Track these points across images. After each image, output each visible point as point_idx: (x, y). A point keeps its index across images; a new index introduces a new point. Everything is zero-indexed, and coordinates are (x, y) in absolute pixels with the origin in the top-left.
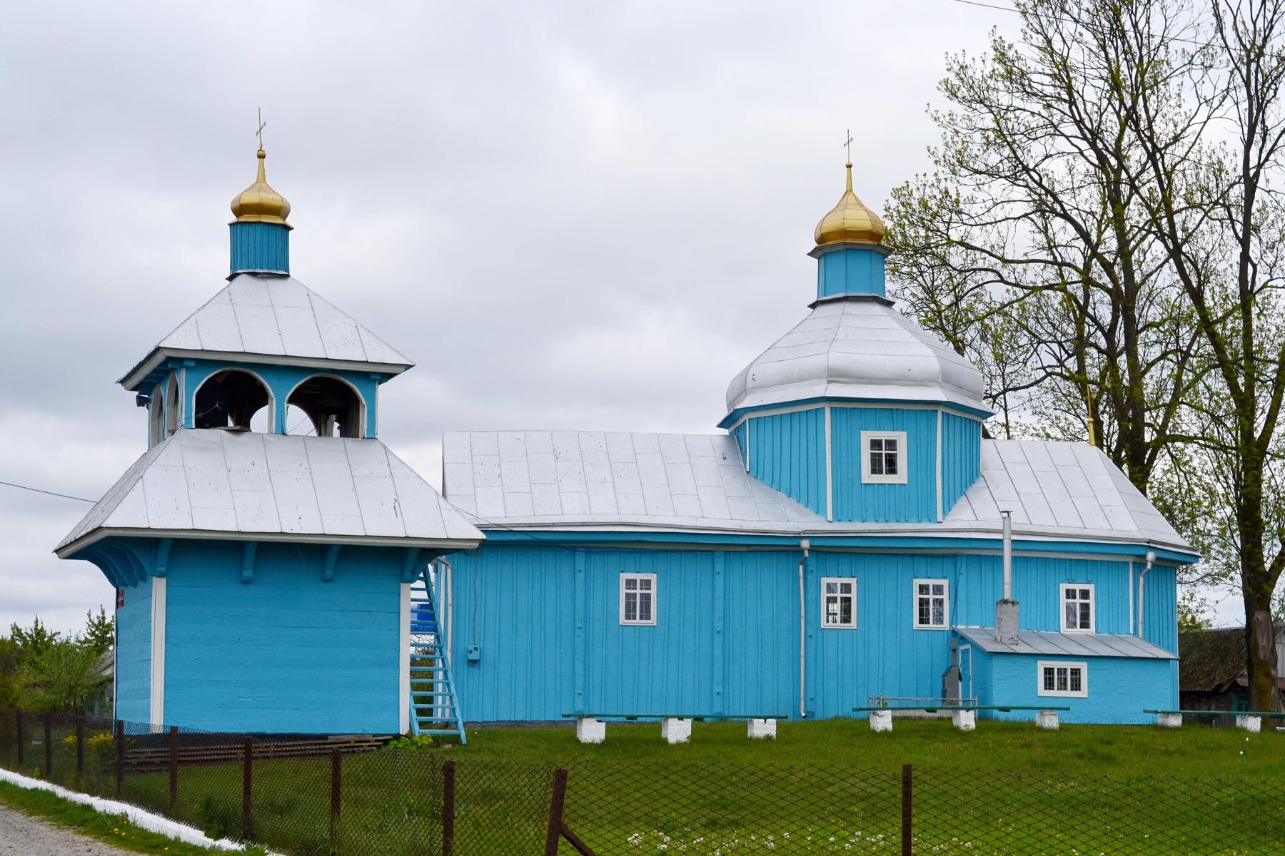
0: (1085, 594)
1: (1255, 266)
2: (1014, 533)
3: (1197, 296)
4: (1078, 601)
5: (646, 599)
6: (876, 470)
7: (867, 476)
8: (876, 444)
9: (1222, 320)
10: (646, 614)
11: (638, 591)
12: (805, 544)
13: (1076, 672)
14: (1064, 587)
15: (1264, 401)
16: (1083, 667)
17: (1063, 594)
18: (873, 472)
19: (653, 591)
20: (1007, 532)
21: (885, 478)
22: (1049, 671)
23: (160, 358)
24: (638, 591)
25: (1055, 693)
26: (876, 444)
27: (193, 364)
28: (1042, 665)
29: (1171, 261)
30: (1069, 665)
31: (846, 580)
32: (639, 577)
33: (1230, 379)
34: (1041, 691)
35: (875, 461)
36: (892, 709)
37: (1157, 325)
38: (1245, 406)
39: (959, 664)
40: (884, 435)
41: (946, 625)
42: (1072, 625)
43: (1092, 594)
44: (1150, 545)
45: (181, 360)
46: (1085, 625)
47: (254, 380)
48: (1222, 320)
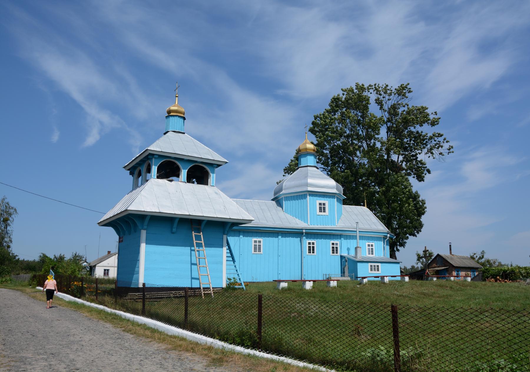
0: (260, 242)
6: (320, 211)
7: (318, 213)
8: (320, 204)
10: (260, 251)
12: (304, 231)
13: (378, 266)
14: (367, 243)
16: (379, 264)
19: (262, 244)
21: (322, 213)
22: (371, 266)
23: (146, 154)
24: (257, 244)
25: (373, 272)
26: (320, 204)
27: (157, 156)
28: (370, 264)
30: (376, 264)
31: (313, 241)
32: (370, 244)
35: (320, 208)
39: (348, 265)
40: (322, 202)
42: (369, 254)
45: (153, 155)
46: (372, 254)
47: (176, 164)
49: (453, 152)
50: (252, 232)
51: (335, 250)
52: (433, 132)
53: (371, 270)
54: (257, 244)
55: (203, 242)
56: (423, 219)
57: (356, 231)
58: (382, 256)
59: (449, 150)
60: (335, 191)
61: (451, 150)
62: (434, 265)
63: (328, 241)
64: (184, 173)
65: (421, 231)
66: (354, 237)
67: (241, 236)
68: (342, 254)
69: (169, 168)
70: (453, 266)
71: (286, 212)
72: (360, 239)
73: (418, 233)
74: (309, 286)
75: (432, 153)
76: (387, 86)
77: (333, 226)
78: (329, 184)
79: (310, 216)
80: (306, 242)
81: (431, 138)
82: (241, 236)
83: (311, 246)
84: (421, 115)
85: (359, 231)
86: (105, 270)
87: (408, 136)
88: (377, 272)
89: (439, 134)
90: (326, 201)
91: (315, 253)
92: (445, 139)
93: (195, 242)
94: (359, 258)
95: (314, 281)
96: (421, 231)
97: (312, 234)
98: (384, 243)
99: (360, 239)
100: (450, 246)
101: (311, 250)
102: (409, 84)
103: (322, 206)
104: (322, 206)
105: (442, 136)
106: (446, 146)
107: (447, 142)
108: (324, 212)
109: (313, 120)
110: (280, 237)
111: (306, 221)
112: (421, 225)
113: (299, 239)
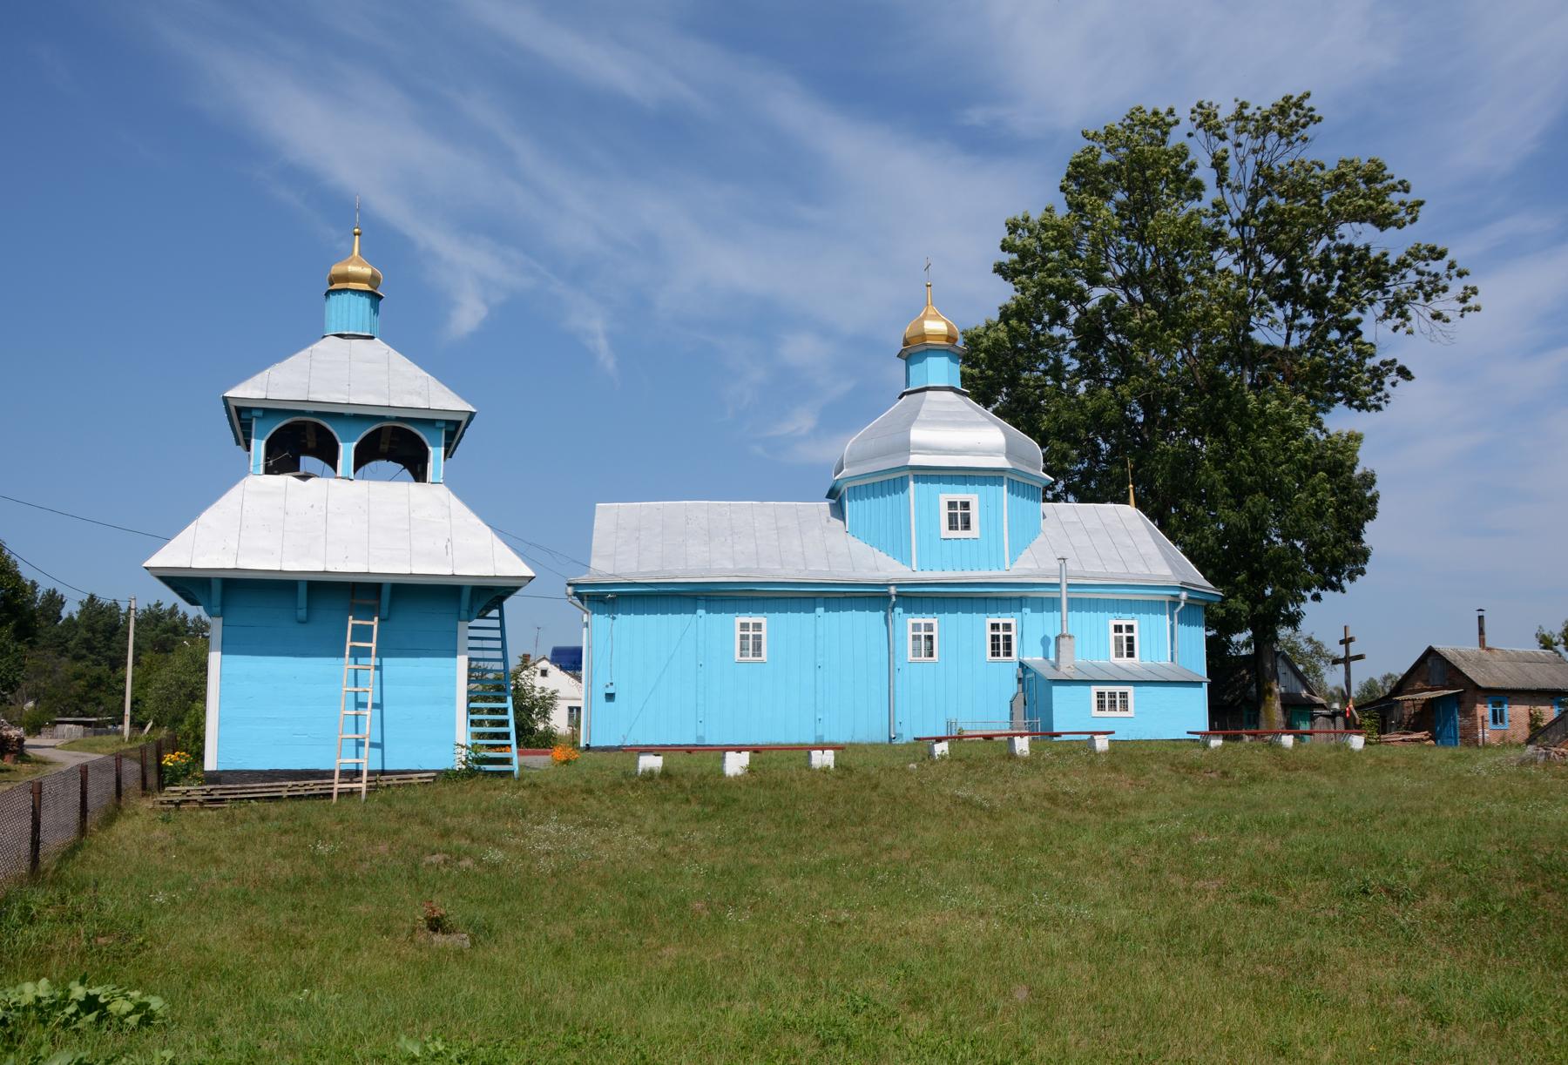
4: (1125, 634)
5: (758, 638)
7: (945, 531)
8: (952, 505)
11: (751, 633)
12: (893, 590)
13: (1123, 695)
16: (1130, 689)
17: (1112, 629)
18: (951, 528)
19: (764, 633)
21: (960, 534)
22: (1100, 695)
24: (751, 633)
25: (1107, 713)
26: (952, 505)
28: (1095, 689)
30: (1118, 689)
32: (1124, 623)
34: (1095, 712)
42: (1119, 654)
46: (1131, 655)
49: (1477, 309)
50: (735, 599)
51: (1001, 645)
52: (1409, 246)
53: (1101, 706)
55: (373, 645)
56: (1371, 534)
57: (1057, 585)
58: (1165, 660)
59: (1464, 300)
60: (1001, 462)
61: (1472, 302)
62: (1418, 685)
63: (977, 617)
64: (346, 452)
65: (1362, 572)
66: (1052, 604)
67: (701, 612)
68: (1026, 659)
69: (299, 441)
70: (1478, 688)
71: (853, 532)
72: (1070, 609)
73: (1352, 579)
74: (735, 764)
75: (1403, 315)
76: (1244, 106)
77: (995, 572)
78: (984, 437)
79: (915, 543)
80: (908, 623)
81: (1402, 264)
82: (701, 612)
83: (1001, 633)
84: (1369, 191)
85: (1069, 586)
86: (571, 709)
87: (1321, 266)
88: (1118, 713)
89: (1432, 250)
90: (971, 495)
92: (1451, 266)
93: (349, 644)
94: (1065, 671)
95: (756, 750)
96: (1362, 572)
97: (918, 598)
98: (1172, 618)
99: (1070, 609)
100: (1481, 618)
101: (928, 644)
102: (1308, 95)
105: (1441, 255)
106: (1456, 287)
107: (1460, 274)
109: (1005, 234)
110: (820, 610)
111: (905, 559)
112: (1365, 555)
113: (882, 613)
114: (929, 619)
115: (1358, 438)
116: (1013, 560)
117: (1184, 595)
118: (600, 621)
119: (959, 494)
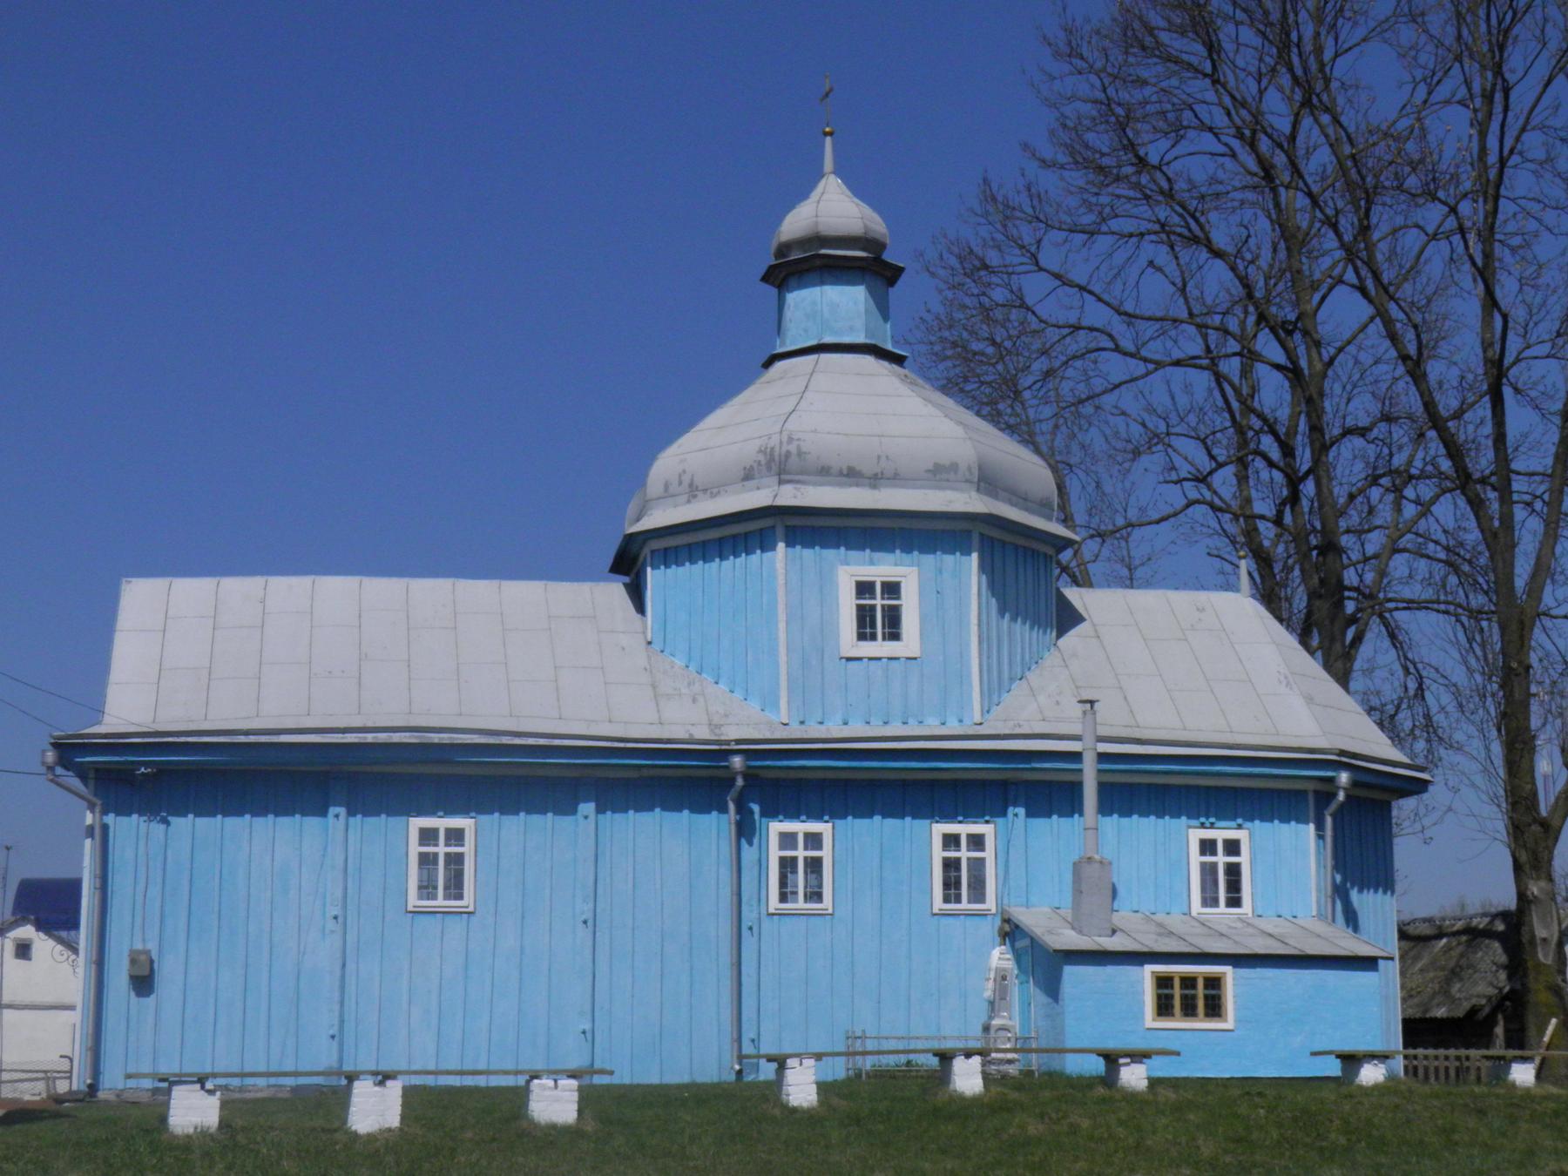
0: (1233, 847)
1: (1505, 317)
2: (1101, 739)
3: (1415, 368)
4: (1221, 859)
6: (865, 629)
8: (864, 589)
9: (1458, 415)
10: (455, 887)
12: (737, 762)
13: (1214, 983)
15: (1529, 531)
16: (1227, 971)
17: (1194, 848)
18: (862, 637)
20: (1089, 740)
21: (880, 648)
22: (1163, 982)
24: (441, 849)
26: (864, 589)
28: (1149, 969)
29: (1378, 320)
31: (1232, 834)
32: (1220, 834)
33: (1477, 505)
35: (865, 618)
36: (818, 1057)
37: (1362, 432)
38: (1500, 540)
41: (991, 904)
43: (989, 843)
44: (1345, 759)
46: (1235, 902)
48: (1458, 415)
54: (441, 849)
72: (1105, 808)
85: (1103, 757)
90: (905, 571)
91: (1247, 907)
98: (1320, 827)
103: (879, 602)
104: (879, 602)
108: (894, 635)
114: (822, 827)
115: (1081, 815)
116: (994, 690)
117: (1344, 777)
118: (128, 829)
119: (881, 568)
